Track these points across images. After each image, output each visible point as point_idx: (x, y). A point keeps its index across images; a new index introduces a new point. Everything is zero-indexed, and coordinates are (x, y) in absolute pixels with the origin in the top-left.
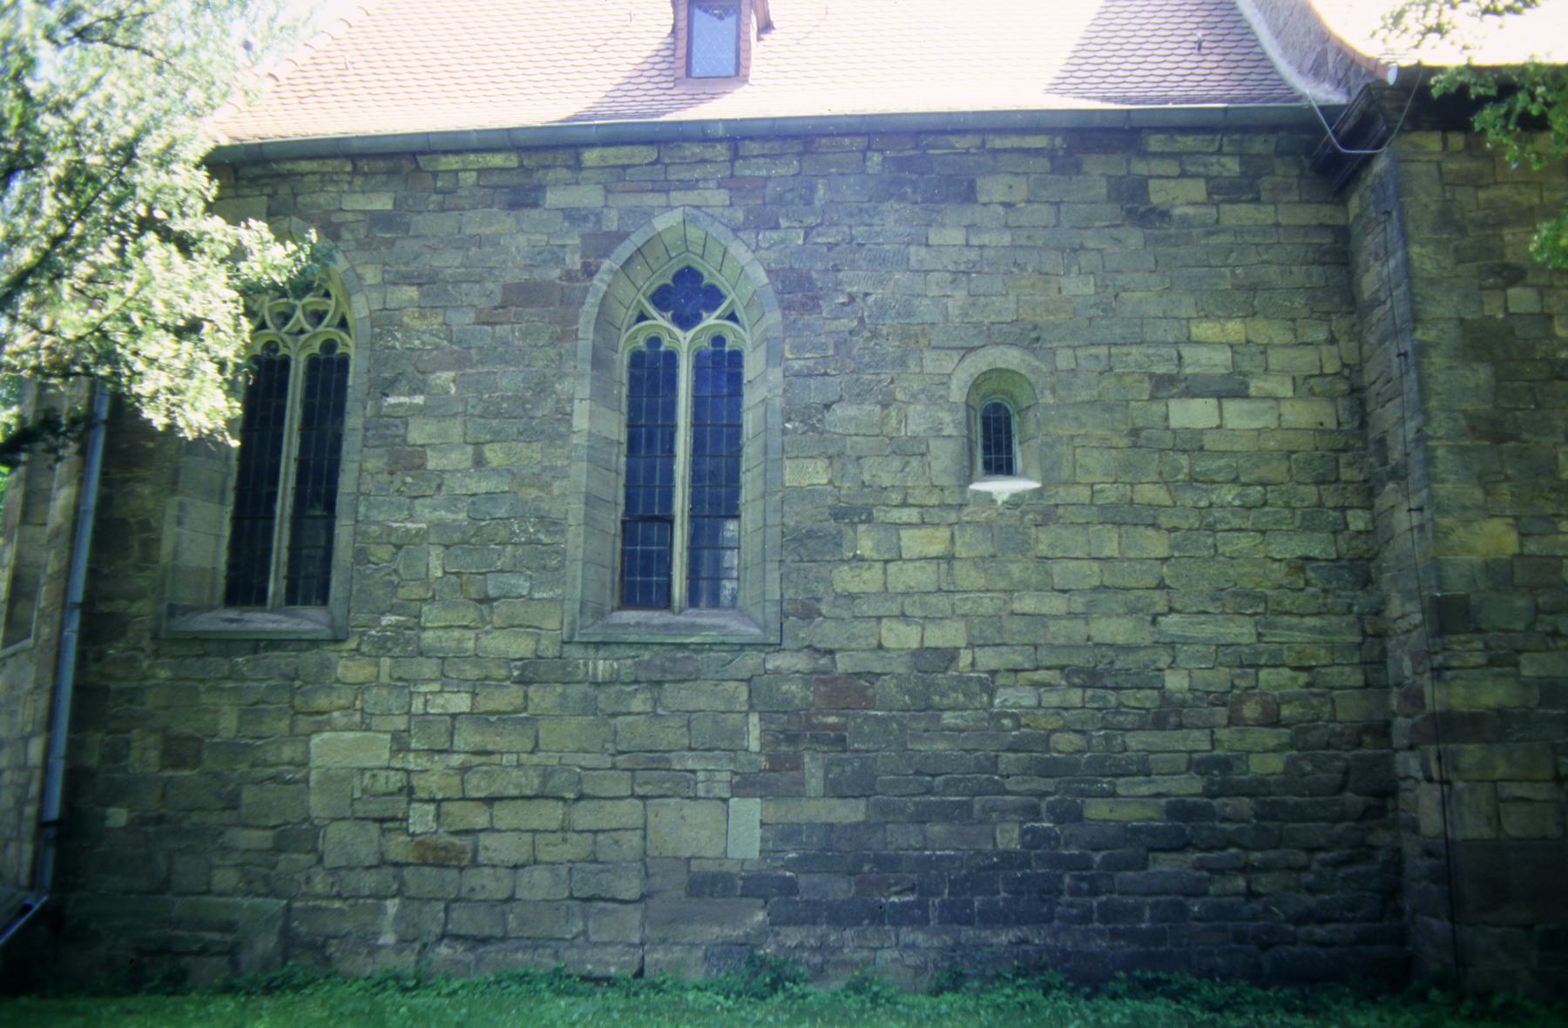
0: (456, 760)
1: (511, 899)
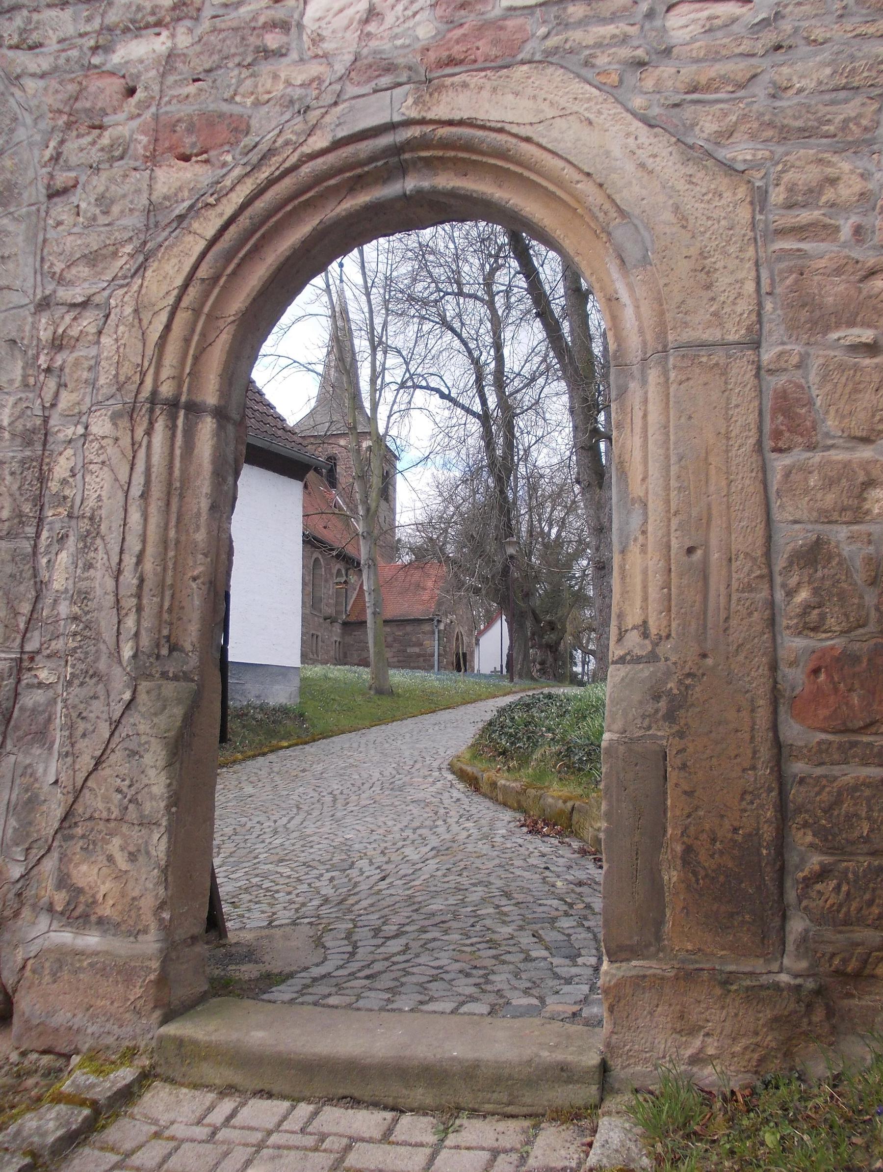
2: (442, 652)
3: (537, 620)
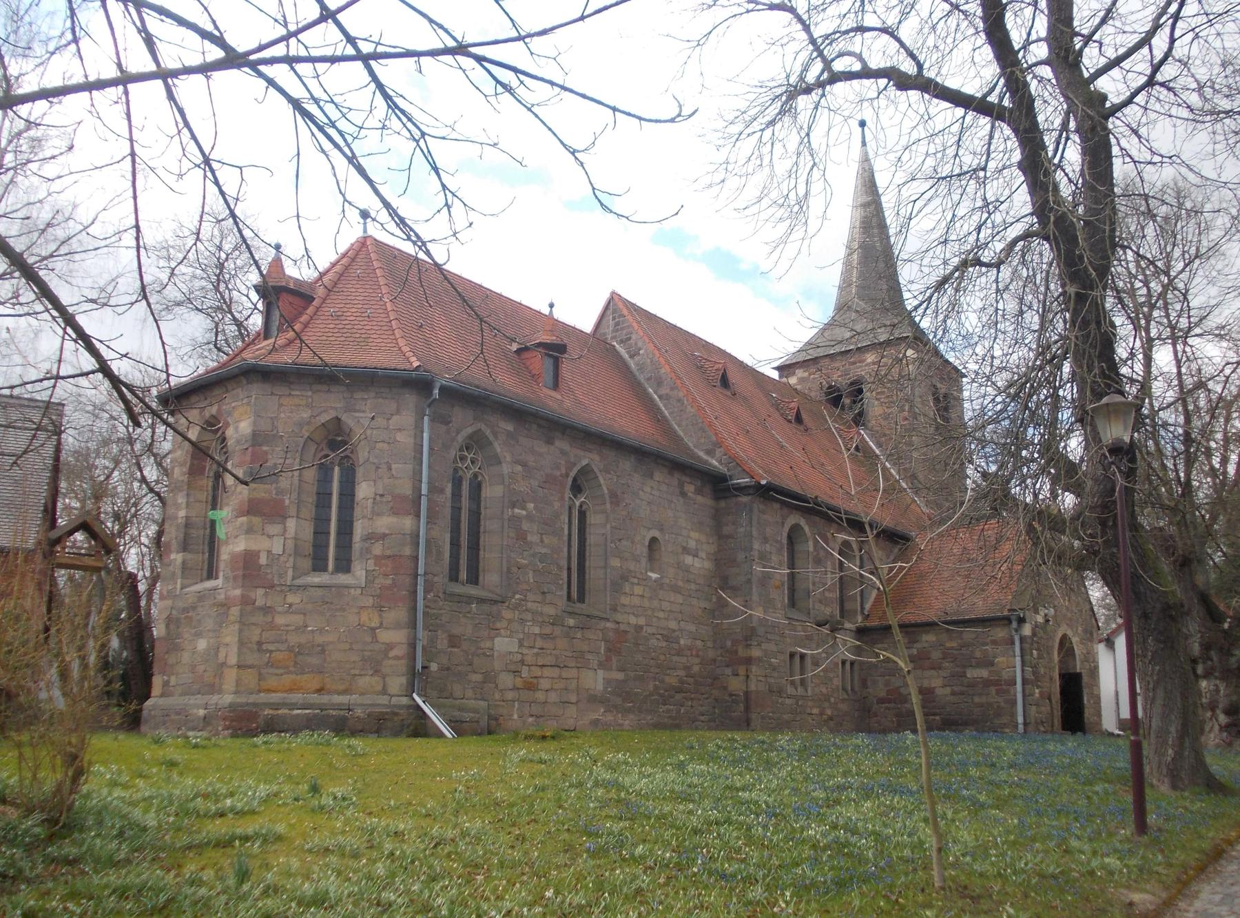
0: (535, 651)
2: (1029, 676)
3: (1214, 616)
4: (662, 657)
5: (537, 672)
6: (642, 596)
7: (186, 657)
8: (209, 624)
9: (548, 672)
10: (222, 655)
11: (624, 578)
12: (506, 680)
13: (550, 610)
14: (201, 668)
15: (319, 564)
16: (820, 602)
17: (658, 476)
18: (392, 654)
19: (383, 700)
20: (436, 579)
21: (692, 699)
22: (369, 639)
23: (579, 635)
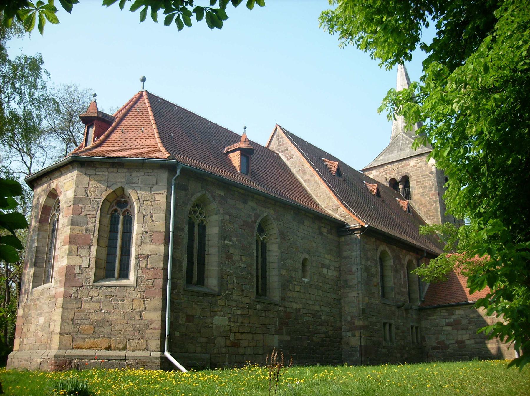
0: (238, 324)
1: (244, 354)
4: (311, 327)
5: (239, 336)
6: (300, 292)
7: (33, 328)
8: (46, 308)
9: (245, 336)
10: (52, 327)
11: (289, 281)
12: (221, 341)
13: (248, 301)
14: (40, 334)
15: (109, 275)
16: (399, 294)
17: (306, 223)
18: (152, 326)
19: (146, 354)
20: (178, 282)
21: (329, 350)
22: (137, 317)
23: (263, 315)
